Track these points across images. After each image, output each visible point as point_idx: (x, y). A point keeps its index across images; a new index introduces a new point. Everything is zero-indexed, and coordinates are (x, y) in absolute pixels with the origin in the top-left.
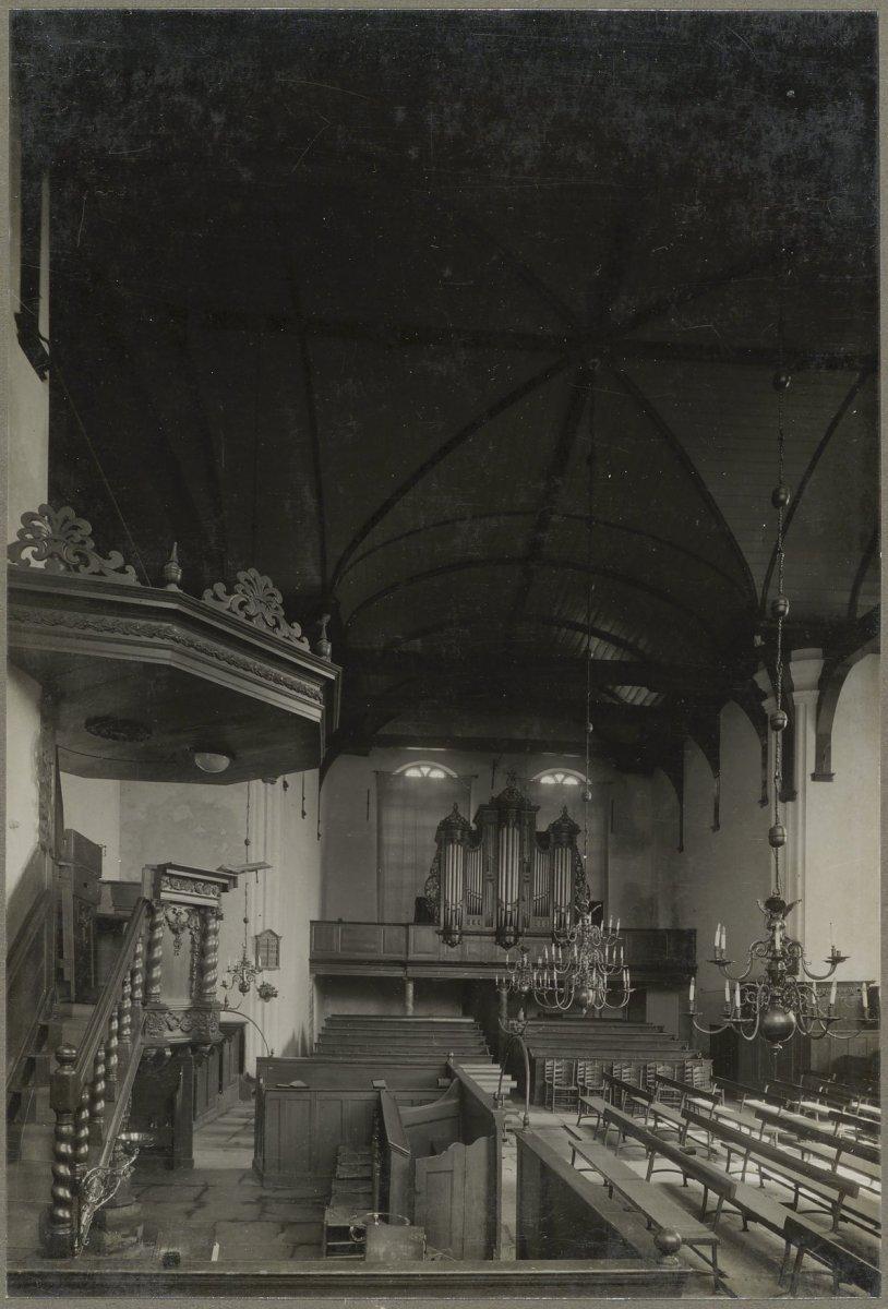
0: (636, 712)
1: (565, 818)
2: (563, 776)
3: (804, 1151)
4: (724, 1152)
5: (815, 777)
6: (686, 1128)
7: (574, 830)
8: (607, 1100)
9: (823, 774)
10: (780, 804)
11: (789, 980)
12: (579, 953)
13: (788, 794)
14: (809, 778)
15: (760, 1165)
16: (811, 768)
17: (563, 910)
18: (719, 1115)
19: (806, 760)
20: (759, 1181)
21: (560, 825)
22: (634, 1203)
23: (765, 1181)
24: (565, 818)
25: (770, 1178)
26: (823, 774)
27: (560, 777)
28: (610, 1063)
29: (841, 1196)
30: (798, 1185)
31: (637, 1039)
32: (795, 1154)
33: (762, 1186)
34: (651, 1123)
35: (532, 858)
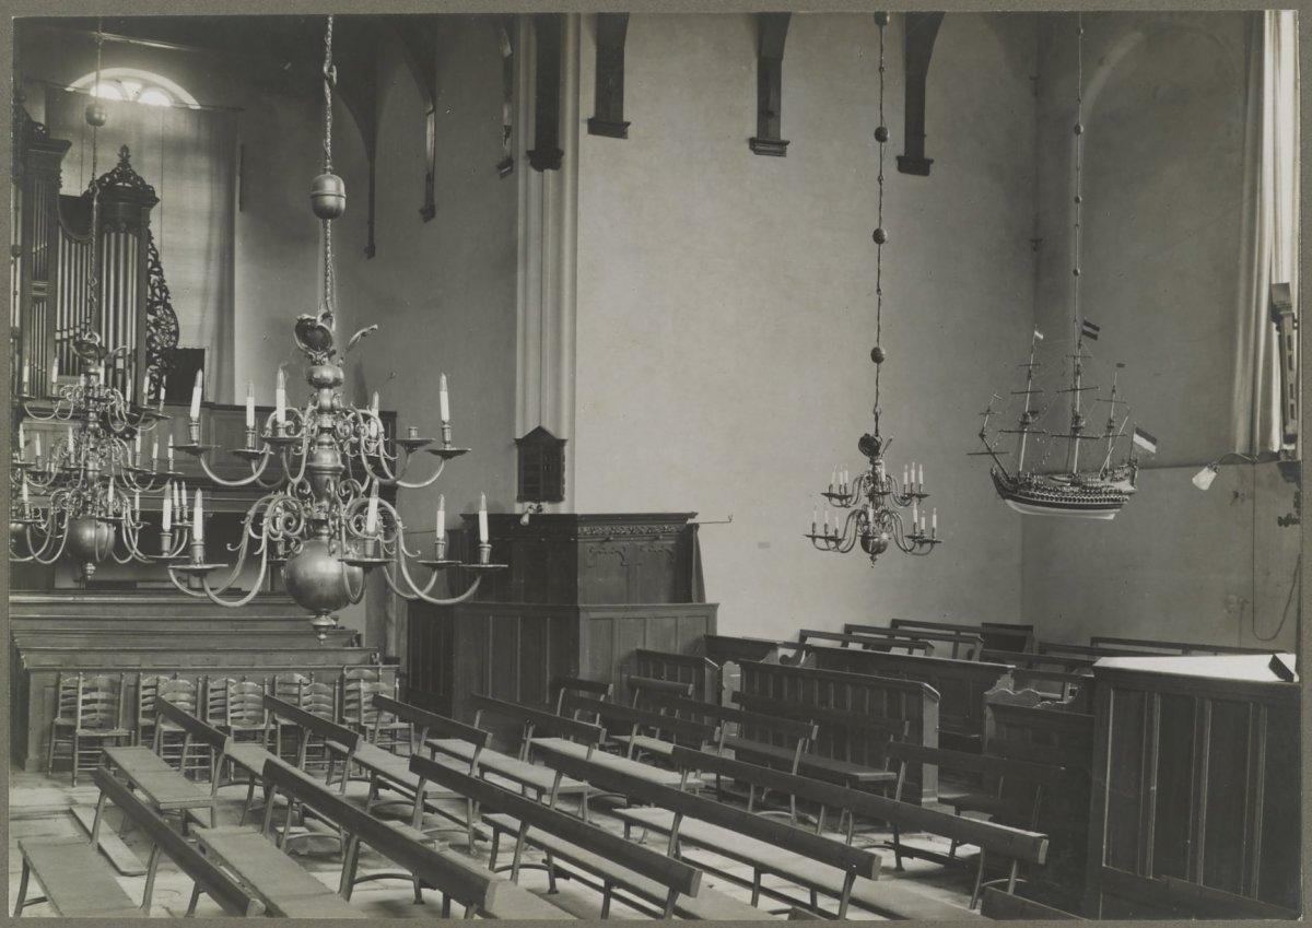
0: (1037, 339)
1: (124, 170)
2: (138, 87)
3: (630, 822)
4: (488, 831)
5: (596, 127)
6: (374, 790)
7: (145, 198)
8: (272, 750)
9: (609, 122)
10: (534, 173)
11: (112, 436)
12: (78, 444)
13: (548, 155)
14: (584, 127)
15: (552, 852)
16: (588, 109)
17: (120, 364)
18: (484, 768)
19: (582, 100)
20: (411, 893)
21: (113, 181)
22: (548, 900)
23: (560, 882)
24: (124, 170)
25: (567, 875)
26: (609, 122)
27: (131, 88)
28: (52, 676)
29: (673, 894)
30: (611, 881)
31: (261, 628)
32: (614, 827)
33: (553, 890)
34: (362, 789)
35: (52, 249)
